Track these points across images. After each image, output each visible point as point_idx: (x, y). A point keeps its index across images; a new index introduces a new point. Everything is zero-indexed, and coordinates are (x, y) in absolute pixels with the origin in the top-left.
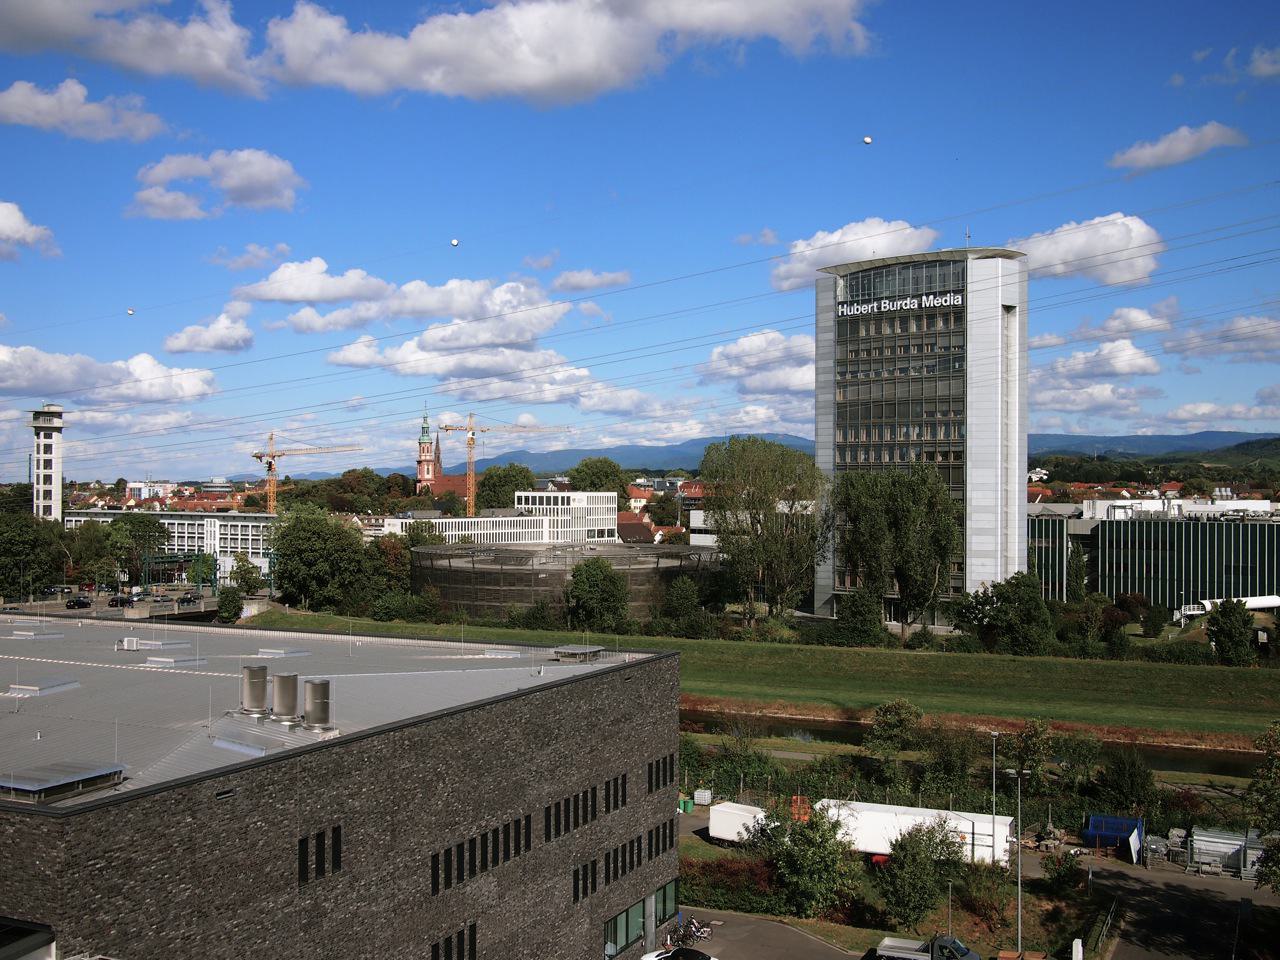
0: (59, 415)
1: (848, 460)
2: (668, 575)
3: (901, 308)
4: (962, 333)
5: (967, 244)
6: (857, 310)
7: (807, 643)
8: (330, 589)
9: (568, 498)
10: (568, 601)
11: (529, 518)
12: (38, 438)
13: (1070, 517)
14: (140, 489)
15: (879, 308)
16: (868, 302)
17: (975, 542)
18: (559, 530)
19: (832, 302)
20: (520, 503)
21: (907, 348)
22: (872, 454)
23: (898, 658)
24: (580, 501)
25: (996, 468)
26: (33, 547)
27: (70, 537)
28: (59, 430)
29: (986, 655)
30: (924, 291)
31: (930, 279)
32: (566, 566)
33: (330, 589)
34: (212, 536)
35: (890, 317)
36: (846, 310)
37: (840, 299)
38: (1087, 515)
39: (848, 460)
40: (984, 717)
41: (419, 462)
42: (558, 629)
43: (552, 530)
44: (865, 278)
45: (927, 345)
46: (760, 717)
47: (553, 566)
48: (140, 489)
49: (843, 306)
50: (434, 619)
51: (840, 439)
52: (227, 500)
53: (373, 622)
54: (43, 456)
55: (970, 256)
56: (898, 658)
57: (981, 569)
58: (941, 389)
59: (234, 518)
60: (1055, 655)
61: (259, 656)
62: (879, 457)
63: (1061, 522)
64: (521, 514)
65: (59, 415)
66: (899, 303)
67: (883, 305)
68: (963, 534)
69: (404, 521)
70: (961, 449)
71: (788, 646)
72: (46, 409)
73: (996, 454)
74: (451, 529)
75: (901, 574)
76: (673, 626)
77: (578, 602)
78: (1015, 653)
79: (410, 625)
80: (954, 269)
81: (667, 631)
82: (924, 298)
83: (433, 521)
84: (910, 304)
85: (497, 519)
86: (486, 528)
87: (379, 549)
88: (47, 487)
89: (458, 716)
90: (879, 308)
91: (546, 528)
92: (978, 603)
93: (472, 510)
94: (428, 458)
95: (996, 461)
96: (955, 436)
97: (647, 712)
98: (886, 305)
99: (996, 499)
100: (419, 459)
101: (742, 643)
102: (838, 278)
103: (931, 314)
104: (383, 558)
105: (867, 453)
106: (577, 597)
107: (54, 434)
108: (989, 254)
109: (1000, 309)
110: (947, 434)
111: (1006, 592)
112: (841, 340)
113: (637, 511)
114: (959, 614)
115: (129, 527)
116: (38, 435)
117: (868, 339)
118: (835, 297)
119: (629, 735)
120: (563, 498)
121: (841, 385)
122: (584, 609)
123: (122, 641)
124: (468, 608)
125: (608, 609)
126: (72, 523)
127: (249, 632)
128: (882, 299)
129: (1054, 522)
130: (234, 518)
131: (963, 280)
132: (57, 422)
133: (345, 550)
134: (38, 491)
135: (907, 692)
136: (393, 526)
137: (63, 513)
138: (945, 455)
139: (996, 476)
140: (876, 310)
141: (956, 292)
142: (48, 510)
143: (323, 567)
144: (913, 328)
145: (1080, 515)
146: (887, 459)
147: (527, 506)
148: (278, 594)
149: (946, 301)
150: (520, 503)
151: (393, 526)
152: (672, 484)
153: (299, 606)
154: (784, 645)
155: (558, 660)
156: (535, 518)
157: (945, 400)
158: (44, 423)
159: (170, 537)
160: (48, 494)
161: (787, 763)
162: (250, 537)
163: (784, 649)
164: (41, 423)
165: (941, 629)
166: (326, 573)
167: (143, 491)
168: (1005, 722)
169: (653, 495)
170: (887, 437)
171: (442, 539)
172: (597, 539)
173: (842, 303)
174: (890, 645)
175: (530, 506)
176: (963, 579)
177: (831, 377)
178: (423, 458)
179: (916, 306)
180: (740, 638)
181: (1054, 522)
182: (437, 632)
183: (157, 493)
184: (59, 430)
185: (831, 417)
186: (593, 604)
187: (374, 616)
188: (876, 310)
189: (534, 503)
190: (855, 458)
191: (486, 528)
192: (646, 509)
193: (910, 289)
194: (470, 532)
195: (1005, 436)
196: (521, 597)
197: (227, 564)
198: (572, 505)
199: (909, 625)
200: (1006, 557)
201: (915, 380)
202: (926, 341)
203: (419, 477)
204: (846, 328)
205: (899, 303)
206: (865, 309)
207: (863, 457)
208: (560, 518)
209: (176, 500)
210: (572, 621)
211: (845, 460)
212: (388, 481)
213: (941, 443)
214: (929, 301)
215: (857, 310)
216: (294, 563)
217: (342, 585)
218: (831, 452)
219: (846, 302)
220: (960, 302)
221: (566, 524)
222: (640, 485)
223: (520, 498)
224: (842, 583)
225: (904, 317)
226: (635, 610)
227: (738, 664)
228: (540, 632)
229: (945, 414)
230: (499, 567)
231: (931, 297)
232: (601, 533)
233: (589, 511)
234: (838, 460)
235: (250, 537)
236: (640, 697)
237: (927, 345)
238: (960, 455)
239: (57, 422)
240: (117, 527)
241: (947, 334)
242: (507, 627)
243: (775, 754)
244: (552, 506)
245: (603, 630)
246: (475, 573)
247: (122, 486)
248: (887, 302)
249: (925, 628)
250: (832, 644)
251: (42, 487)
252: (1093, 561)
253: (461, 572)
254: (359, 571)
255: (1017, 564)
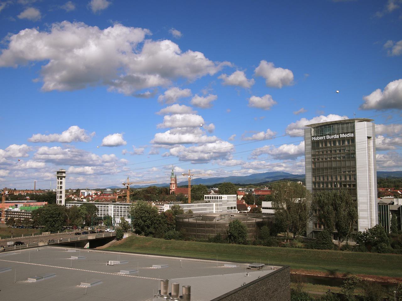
0: (64, 172)
1: (317, 187)
2: (259, 225)
3: (333, 138)
4: (354, 146)
5: (354, 117)
6: (319, 138)
7: (308, 248)
8: (151, 230)
9: (221, 197)
10: (228, 233)
11: (209, 203)
12: (58, 179)
13: (389, 204)
14: (84, 192)
15: (326, 138)
16: (322, 136)
17: (361, 214)
18: (219, 207)
19: (310, 136)
20: (206, 198)
21: (335, 151)
22: (325, 185)
23: (339, 254)
24: (225, 198)
25: (367, 190)
26: (59, 215)
27: (66, 210)
28: (64, 177)
29: (369, 253)
30: (341, 133)
31: (343, 129)
32: (226, 221)
33: (151, 230)
34: (111, 210)
35: (330, 141)
36: (314, 139)
37: (313, 135)
38: (395, 203)
39: (317, 187)
40: (371, 275)
41: (171, 184)
42: (225, 243)
43: (216, 207)
44: (321, 128)
45: (342, 150)
46: (295, 274)
47: (221, 221)
48: (84, 192)
49: (314, 138)
50: (185, 239)
51: (314, 180)
52: (111, 196)
53: (165, 240)
54: (60, 185)
55: (356, 121)
56: (339, 254)
57: (363, 223)
58: (348, 164)
59: (118, 204)
60: (393, 253)
61: (153, 268)
62: (327, 186)
63: (387, 206)
64: (207, 202)
65: (64, 172)
66: (332, 136)
67: (327, 137)
68: (357, 211)
69: (170, 205)
70: (355, 183)
71: (301, 249)
72: (61, 171)
73: (367, 185)
74: (186, 207)
75: (338, 226)
76: (262, 242)
77: (231, 234)
78: (378, 252)
79: (177, 241)
80: (351, 125)
81: (260, 244)
82: (341, 135)
83: (180, 205)
84: (337, 136)
85: (199, 204)
86: (196, 208)
87: (165, 215)
88: (61, 195)
89: (230, 296)
90: (326, 138)
91: (214, 207)
92: (364, 235)
93: (190, 200)
94: (174, 182)
95: (367, 187)
96: (352, 179)
97: (282, 287)
98: (328, 137)
99: (368, 200)
100: (171, 183)
101: (285, 248)
102: (312, 128)
103: (343, 140)
104: (166, 218)
105: (323, 184)
106: (231, 232)
107: (63, 178)
108: (362, 120)
109: (366, 137)
110: (350, 178)
111: (373, 231)
112: (313, 148)
113: (240, 199)
114: (358, 238)
115: (86, 208)
116: (58, 178)
117: (322, 148)
118: (311, 134)
119: (277, 296)
120: (220, 197)
121: (314, 163)
122: (233, 236)
123: (108, 262)
124: (195, 235)
125: (241, 236)
126: (69, 206)
127: (143, 255)
128: (327, 135)
129: (385, 206)
130: (118, 204)
131: (354, 129)
132: (64, 175)
133: (155, 217)
134: (58, 196)
135: (343, 266)
136: (166, 208)
137: (65, 202)
138: (350, 185)
139: (367, 192)
140: (325, 139)
141: (351, 133)
142: (61, 202)
143: (149, 222)
144: (337, 144)
145: (393, 203)
146: (330, 186)
147: (208, 200)
148: (134, 230)
149: (348, 136)
150: (206, 198)
151: (166, 208)
152: (250, 190)
153: (141, 234)
154: (300, 249)
155: (250, 269)
156: (211, 203)
157: (349, 167)
158: (60, 175)
159: (98, 211)
160: (61, 197)
161: (314, 295)
162: (123, 211)
163: (300, 250)
164: (59, 175)
165: (352, 243)
166: (150, 224)
167: (85, 193)
168: (380, 277)
169: (245, 194)
170: (330, 179)
171: (182, 211)
172: (230, 210)
173: (313, 136)
174: (335, 249)
175: (209, 199)
176: (357, 226)
177: (310, 160)
178: (172, 182)
179: (338, 137)
180: (285, 247)
181: (385, 206)
182: (186, 244)
183: (90, 193)
184: (64, 177)
185: (311, 173)
186: (236, 235)
187: (165, 238)
188: (325, 139)
189: (210, 199)
190: (319, 186)
191: (196, 208)
192: (243, 198)
193: (336, 132)
194: (191, 208)
195: (369, 179)
196: (212, 232)
197: (118, 220)
198: (223, 199)
199: (341, 242)
200: (371, 219)
201: (338, 161)
202: (342, 148)
203: (171, 188)
204: (315, 145)
205: (332, 136)
206: (321, 138)
207: (322, 186)
208: (219, 203)
209: (96, 196)
210: (229, 240)
211: (316, 187)
212: (161, 190)
213: (348, 182)
214: (342, 136)
215: (319, 138)
216: (140, 221)
217: (155, 228)
218: (311, 184)
219: (315, 136)
220: (353, 136)
221: (221, 205)
222: (240, 190)
223: (206, 197)
224: (316, 226)
225: (334, 141)
226: (249, 237)
227: (285, 255)
228: (219, 244)
229: (349, 172)
230: (205, 222)
231: (343, 134)
232: (232, 208)
233: (228, 201)
234: (313, 187)
235: (123, 211)
236: (280, 282)
237: (342, 150)
238: (355, 185)
239: (64, 175)
240: (82, 207)
241: (349, 146)
242: (208, 242)
243: (310, 292)
244: (216, 200)
245: (239, 243)
246: (197, 224)
247: (78, 191)
248: (328, 136)
249: (347, 243)
250: (315, 249)
251: (59, 195)
252: (399, 219)
253: (193, 224)
254: (160, 223)
255: (375, 223)
